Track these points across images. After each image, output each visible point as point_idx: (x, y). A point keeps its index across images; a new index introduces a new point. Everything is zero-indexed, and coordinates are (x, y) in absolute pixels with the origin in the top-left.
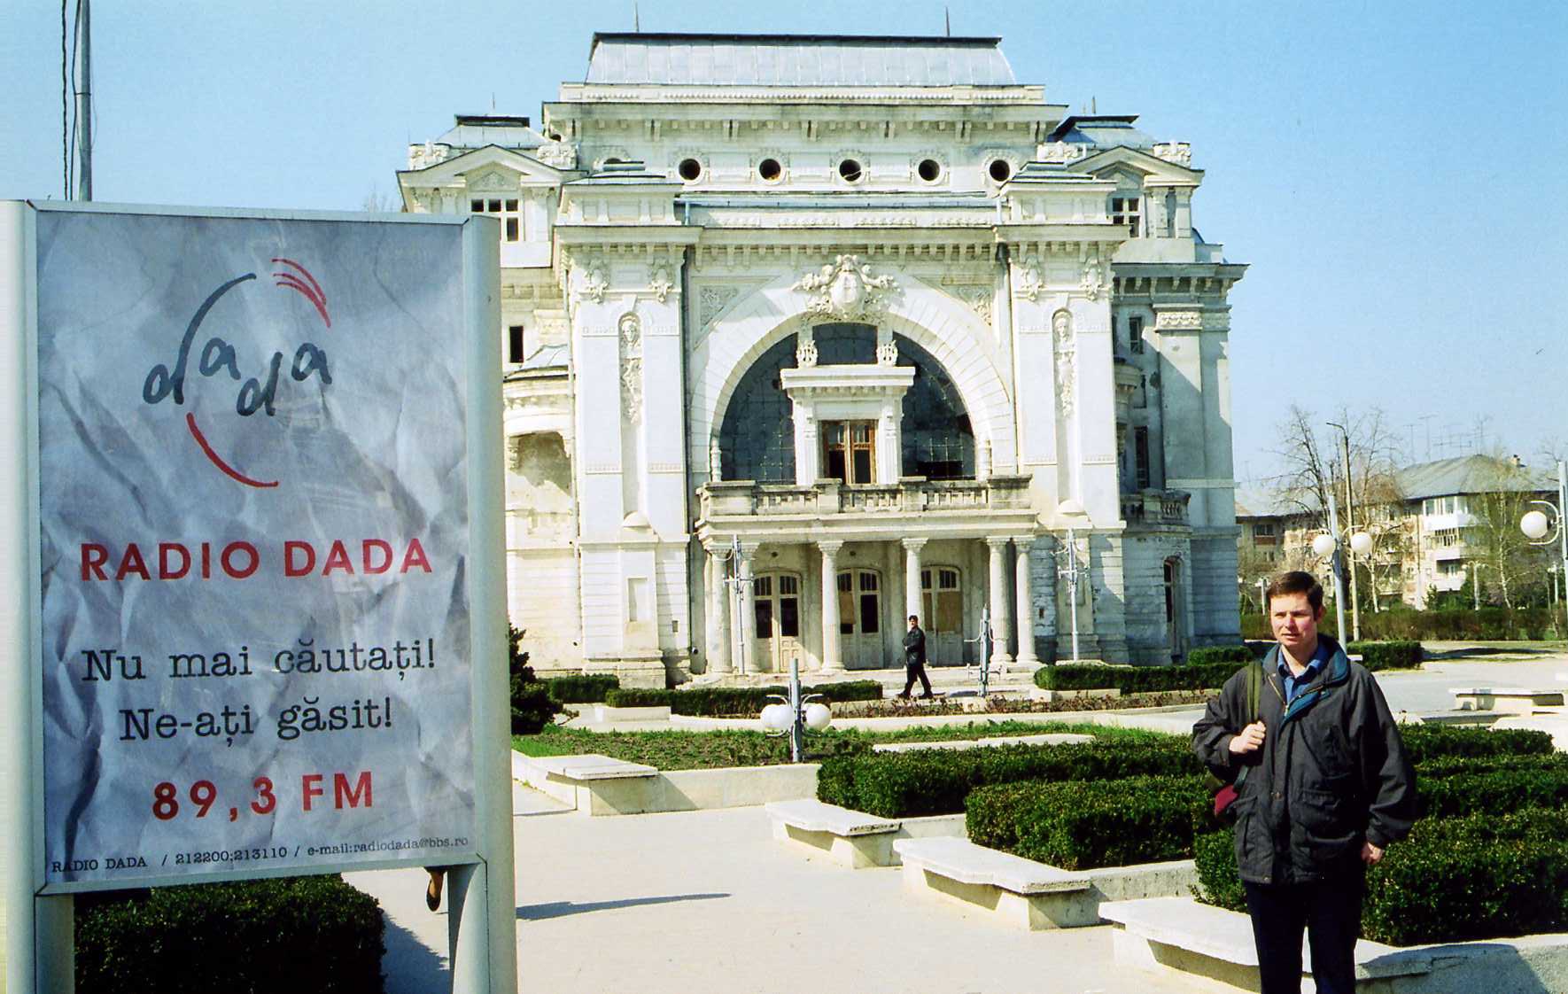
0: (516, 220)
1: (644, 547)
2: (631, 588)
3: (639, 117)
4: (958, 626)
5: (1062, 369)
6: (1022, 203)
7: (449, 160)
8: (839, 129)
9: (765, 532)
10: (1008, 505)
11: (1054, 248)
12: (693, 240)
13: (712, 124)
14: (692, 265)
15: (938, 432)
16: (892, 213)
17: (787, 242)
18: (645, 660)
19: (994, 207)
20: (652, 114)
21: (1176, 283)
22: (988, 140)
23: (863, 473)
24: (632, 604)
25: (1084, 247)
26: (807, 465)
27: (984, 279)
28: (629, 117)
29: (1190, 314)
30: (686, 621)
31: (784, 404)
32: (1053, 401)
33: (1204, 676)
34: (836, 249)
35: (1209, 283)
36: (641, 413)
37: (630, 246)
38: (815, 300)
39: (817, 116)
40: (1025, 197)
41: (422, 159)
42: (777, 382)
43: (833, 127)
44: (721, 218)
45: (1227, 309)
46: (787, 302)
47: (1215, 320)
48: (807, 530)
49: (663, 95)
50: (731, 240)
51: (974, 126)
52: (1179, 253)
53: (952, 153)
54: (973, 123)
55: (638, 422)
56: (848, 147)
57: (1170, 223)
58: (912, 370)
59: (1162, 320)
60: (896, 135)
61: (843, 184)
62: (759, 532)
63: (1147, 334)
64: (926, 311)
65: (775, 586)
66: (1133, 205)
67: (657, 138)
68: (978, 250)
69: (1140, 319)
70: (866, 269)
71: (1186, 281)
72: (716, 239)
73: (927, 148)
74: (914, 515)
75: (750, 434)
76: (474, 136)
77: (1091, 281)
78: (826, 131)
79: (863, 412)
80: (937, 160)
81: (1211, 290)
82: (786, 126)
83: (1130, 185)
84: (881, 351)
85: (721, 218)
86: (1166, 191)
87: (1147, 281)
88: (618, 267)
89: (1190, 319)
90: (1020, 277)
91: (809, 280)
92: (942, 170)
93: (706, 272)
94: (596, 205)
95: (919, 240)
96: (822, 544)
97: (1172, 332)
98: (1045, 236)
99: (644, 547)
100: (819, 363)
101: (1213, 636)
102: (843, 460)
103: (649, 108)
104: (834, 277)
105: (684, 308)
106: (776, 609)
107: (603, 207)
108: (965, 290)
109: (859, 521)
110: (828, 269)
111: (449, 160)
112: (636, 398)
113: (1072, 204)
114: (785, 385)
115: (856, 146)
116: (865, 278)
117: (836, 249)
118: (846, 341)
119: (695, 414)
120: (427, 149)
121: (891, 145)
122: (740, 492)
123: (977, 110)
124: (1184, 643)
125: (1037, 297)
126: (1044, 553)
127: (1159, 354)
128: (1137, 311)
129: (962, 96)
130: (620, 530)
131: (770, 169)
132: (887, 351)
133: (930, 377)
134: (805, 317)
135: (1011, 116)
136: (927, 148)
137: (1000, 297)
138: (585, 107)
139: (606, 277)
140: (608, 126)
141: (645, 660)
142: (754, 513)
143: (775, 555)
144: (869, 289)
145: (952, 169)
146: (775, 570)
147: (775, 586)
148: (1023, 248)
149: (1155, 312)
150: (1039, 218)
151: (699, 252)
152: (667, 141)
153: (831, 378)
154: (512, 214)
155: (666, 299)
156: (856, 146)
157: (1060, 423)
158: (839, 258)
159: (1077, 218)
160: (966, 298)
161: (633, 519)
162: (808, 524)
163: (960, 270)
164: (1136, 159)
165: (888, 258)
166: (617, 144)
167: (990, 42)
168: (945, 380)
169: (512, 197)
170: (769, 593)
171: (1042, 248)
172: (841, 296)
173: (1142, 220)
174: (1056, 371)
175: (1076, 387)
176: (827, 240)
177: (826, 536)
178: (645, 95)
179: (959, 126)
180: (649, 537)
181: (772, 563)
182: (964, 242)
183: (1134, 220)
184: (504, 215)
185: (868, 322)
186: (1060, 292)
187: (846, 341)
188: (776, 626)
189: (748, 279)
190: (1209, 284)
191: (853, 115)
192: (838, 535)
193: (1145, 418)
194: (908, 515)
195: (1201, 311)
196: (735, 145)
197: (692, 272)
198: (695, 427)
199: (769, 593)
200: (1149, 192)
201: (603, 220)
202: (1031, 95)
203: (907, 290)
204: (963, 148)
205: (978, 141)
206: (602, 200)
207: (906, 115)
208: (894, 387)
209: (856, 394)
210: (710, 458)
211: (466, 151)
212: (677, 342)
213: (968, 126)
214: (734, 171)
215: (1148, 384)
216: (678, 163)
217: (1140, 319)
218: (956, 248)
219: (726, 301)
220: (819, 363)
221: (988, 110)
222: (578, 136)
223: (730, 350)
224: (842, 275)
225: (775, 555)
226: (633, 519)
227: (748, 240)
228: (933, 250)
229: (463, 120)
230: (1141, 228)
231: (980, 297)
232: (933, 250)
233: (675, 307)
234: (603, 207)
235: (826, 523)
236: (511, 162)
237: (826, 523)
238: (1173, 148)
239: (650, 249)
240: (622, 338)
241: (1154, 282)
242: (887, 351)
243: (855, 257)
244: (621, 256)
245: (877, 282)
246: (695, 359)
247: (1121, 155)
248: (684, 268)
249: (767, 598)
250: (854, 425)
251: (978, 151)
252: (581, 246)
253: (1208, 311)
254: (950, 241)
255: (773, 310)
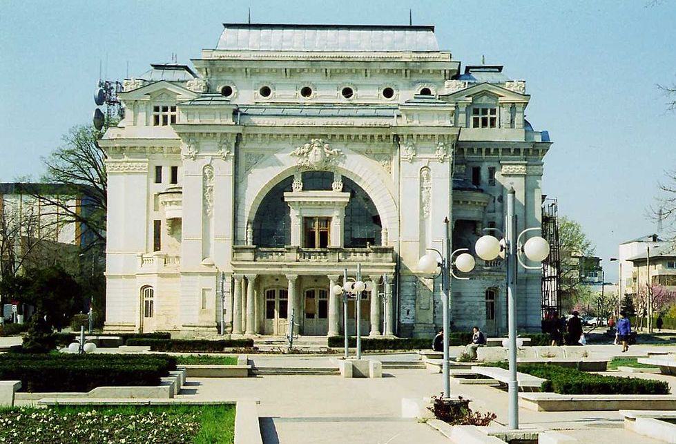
0: (175, 116)
1: (211, 274)
2: (203, 294)
3: (239, 66)
4: (367, 317)
5: (424, 195)
6: (407, 115)
7: (143, 87)
8: (342, 73)
9: (260, 269)
10: (381, 261)
11: (422, 137)
12: (240, 131)
13: (277, 70)
14: (241, 144)
15: (363, 224)
16: (341, 119)
17: (287, 133)
18: (208, 327)
19: (393, 117)
20: (245, 65)
21: (512, 151)
22: (420, 79)
23: (324, 242)
24: (204, 301)
25: (437, 137)
26: (296, 238)
27: (388, 151)
28: (234, 66)
29: (520, 167)
30: (230, 309)
31: (285, 208)
32: (418, 210)
33: (401, 343)
34: (313, 136)
35: (533, 151)
36: (212, 212)
37: (208, 133)
38: (301, 160)
39: (330, 67)
40: (409, 112)
41: (129, 86)
42: (283, 198)
43: (338, 71)
44: (256, 120)
45: (542, 164)
46: (287, 160)
47: (535, 170)
48: (280, 269)
49: (252, 56)
50: (260, 131)
51: (412, 71)
52: (516, 136)
53: (401, 85)
54: (411, 70)
55: (211, 216)
56: (347, 81)
57: (512, 121)
58: (348, 194)
59: (505, 169)
60: (371, 76)
61: (344, 100)
62: (256, 269)
63: (497, 176)
64: (357, 165)
65: (277, 294)
66: (493, 112)
67: (249, 76)
68: (384, 138)
69: (494, 168)
70: (326, 145)
71: (517, 151)
72: (252, 131)
73: (388, 82)
74: (333, 264)
75: (268, 224)
76: (158, 75)
77: (440, 153)
78: (333, 74)
79: (325, 214)
80: (392, 88)
81: (533, 155)
82: (314, 71)
83: (492, 102)
84: (334, 185)
85: (256, 120)
86: (510, 105)
87: (496, 150)
88: (203, 143)
89: (521, 169)
90: (405, 151)
91: (298, 151)
92: (395, 92)
93: (247, 146)
94: (194, 114)
95: (353, 132)
96: (287, 275)
97: (510, 175)
98: (416, 132)
99: (211, 274)
100: (304, 189)
101: (525, 328)
102: (315, 237)
103: (245, 62)
104: (310, 149)
105: (236, 163)
106: (277, 305)
107: (197, 115)
108: (377, 157)
109: (305, 266)
110: (307, 145)
111: (143, 87)
112: (211, 205)
113: (433, 116)
114: (286, 200)
115: (350, 81)
116: (325, 150)
117: (313, 136)
118: (318, 179)
119: (240, 212)
120: (132, 82)
121: (369, 80)
122: (249, 251)
123: (413, 63)
124: (500, 331)
125: (412, 161)
126: (410, 284)
127: (502, 186)
128: (492, 165)
129: (406, 57)
130: (200, 266)
131: (306, 92)
132: (337, 185)
133: (360, 198)
134: (299, 167)
135: (431, 67)
136: (388, 82)
137: (395, 159)
138: (211, 62)
139: (197, 147)
140: (224, 70)
141: (208, 327)
142: (255, 260)
143: (277, 280)
144: (328, 155)
145: (400, 92)
146: (278, 287)
147: (277, 294)
148: (405, 137)
149: (501, 165)
150: (416, 122)
151: (244, 137)
152: (254, 78)
153: (307, 197)
154: (173, 113)
155: (226, 158)
156: (350, 81)
157: (422, 221)
158: (313, 140)
159: (436, 123)
160: (379, 160)
161: (207, 261)
162: (281, 266)
163: (375, 147)
164: (493, 89)
165: (338, 141)
166: (227, 79)
167: (432, 29)
168: (368, 199)
169: (174, 105)
170: (274, 298)
171: (415, 137)
172: (314, 158)
173: (497, 120)
174: (421, 196)
175: (431, 203)
176: (307, 132)
177: (289, 272)
178: (244, 56)
179: (404, 72)
180: (213, 270)
181: (276, 284)
182: (376, 134)
183: (493, 120)
184: (169, 113)
185: (329, 170)
186: (425, 157)
187: (318, 179)
188: (276, 313)
189: (269, 150)
190: (531, 152)
191: (348, 66)
192: (295, 272)
193: (494, 218)
194: (330, 264)
195: (526, 165)
196: (288, 81)
197: (241, 146)
198: (239, 218)
199: (274, 298)
200: (502, 105)
201: (197, 121)
202: (443, 56)
203: (347, 156)
204: (407, 82)
205: (415, 79)
206: (197, 112)
207: (375, 66)
208: (340, 202)
209: (321, 205)
210: (247, 234)
211: (152, 83)
212: (231, 180)
213: (408, 72)
214: (288, 92)
215: (496, 201)
216: (260, 88)
217: (494, 168)
218: (372, 136)
219: (257, 159)
220: (304, 189)
221: (418, 64)
222: (209, 75)
223: (258, 183)
224: (314, 148)
225: (277, 280)
226: (207, 261)
227: (268, 131)
228: (360, 137)
229: (157, 67)
230: (497, 123)
231: (386, 160)
232: (360, 137)
233: (231, 162)
234: (197, 115)
235: (289, 266)
236: (172, 88)
237: (289, 266)
238: (515, 84)
239: (218, 135)
240: (205, 177)
241: (500, 151)
242: (337, 185)
243: (320, 140)
244: (205, 138)
245: (332, 152)
246: (241, 187)
247: (485, 87)
248: (236, 145)
249: (272, 300)
250: (320, 219)
251: (414, 84)
252: (184, 133)
253: (530, 165)
254: (369, 133)
255: (279, 164)
